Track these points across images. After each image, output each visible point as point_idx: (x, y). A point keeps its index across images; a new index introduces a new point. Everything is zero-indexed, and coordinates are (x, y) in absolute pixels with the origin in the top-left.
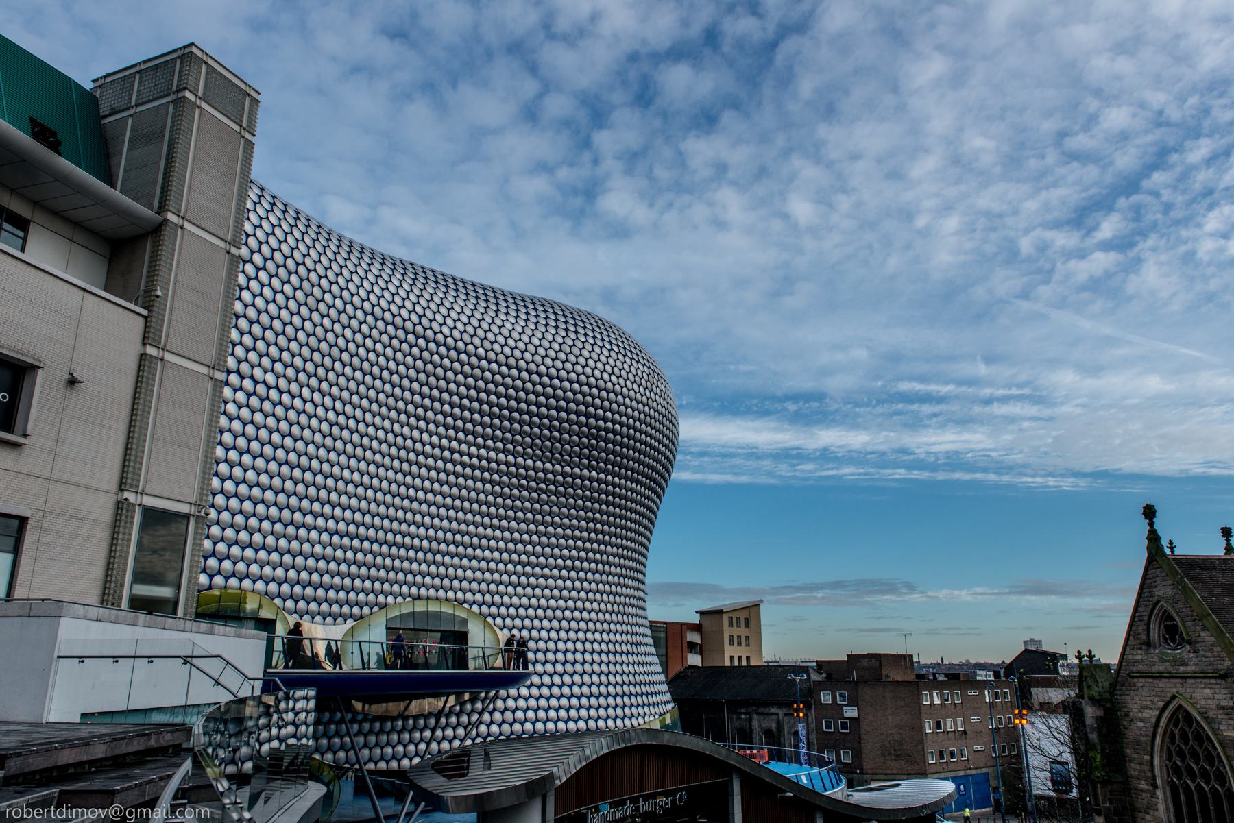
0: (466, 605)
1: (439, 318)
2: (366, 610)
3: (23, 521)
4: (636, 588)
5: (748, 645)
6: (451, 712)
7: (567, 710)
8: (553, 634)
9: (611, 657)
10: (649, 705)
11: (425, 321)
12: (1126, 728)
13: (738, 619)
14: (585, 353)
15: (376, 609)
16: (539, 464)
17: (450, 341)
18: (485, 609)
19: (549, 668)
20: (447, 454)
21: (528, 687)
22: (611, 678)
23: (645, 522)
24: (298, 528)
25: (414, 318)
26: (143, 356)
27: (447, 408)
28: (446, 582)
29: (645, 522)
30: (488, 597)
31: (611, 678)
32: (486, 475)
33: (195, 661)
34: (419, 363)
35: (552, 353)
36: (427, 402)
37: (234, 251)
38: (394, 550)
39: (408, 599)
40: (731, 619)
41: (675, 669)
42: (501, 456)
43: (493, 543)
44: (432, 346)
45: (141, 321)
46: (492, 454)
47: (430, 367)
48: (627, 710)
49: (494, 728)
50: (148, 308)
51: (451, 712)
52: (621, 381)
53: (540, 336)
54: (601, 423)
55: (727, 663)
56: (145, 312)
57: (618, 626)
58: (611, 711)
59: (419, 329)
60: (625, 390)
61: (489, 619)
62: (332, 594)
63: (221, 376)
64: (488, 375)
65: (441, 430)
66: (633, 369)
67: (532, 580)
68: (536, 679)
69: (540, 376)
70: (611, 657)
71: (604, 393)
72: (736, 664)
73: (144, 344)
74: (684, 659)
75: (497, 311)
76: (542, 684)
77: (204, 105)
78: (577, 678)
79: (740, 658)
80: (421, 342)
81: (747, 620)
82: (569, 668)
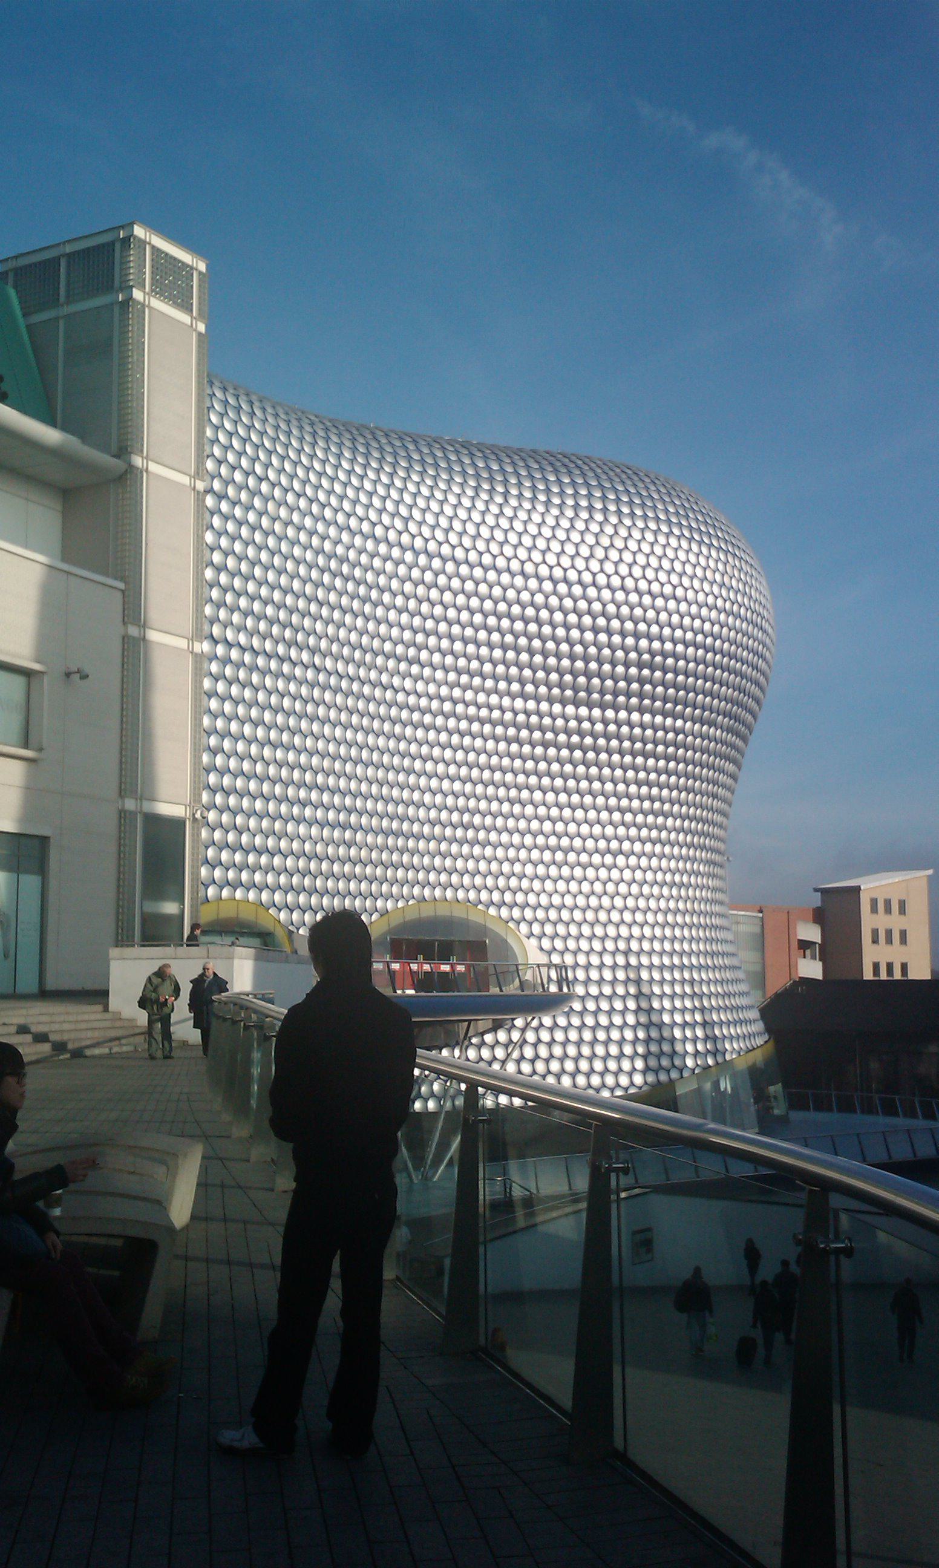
3: (44, 840)
21: (567, 1015)
23: (744, 714)
25: (399, 524)
26: (125, 638)
29: (744, 714)
33: (88, 1052)
40: (874, 903)
41: (777, 983)
45: (119, 595)
49: (562, 1021)
50: (122, 579)
55: (868, 975)
56: (122, 586)
61: (511, 925)
71: (660, 602)
72: (884, 976)
73: (124, 623)
74: (791, 966)
79: (890, 966)
80: (409, 557)
81: (903, 935)
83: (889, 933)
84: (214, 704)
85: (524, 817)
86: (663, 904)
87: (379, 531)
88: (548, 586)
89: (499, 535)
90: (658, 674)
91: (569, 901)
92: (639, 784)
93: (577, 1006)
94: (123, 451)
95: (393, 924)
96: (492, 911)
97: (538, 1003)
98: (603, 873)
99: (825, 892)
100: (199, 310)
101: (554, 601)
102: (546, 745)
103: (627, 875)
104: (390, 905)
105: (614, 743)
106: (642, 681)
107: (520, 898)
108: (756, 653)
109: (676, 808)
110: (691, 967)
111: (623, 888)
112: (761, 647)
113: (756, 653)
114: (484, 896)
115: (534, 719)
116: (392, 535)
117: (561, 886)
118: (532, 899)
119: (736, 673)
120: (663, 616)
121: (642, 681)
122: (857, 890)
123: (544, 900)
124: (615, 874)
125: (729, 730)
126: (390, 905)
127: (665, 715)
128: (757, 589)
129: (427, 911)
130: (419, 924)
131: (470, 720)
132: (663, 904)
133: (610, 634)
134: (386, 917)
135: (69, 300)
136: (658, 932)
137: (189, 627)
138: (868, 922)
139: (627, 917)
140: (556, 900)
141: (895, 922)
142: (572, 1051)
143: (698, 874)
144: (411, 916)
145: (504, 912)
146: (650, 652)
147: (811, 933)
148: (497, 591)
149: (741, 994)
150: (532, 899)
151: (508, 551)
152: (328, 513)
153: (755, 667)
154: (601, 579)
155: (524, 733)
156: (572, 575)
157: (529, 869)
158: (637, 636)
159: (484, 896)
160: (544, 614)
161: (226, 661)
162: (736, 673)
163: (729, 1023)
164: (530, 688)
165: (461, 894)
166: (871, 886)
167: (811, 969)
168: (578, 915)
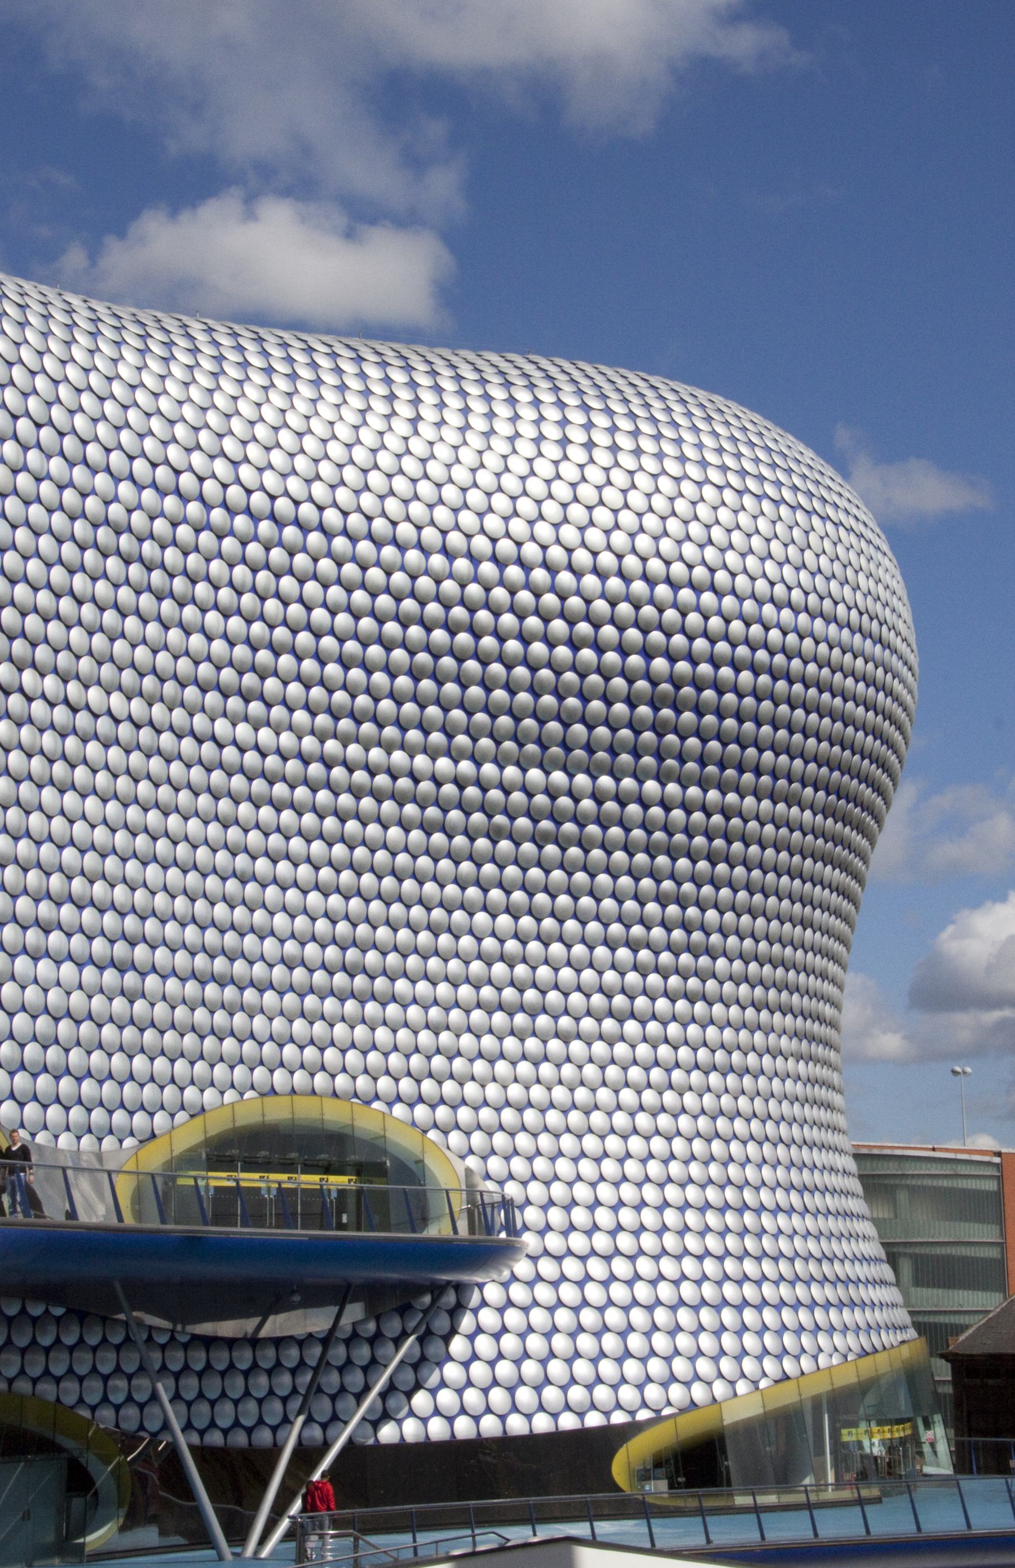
0: (376, 1105)
2: (160, 1118)
4: (799, 1057)
6: (353, 1339)
7: (623, 1335)
8: (586, 1167)
9: (748, 1218)
10: (832, 1329)
12: (72, 1214)
14: (636, 499)
15: (181, 1117)
16: (535, 774)
18: (421, 1112)
19: (578, 1242)
20: (315, 769)
24: (665, 1024)
27: (309, 665)
31: (730, 1265)
32: (410, 809)
35: (551, 509)
38: (211, 990)
39: (249, 1095)
42: (444, 764)
46: (421, 761)
47: (240, 572)
48: (788, 1339)
51: (353, 1339)
57: (781, 1149)
58: (728, 1341)
59: (234, 492)
60: (741, 581)
62: (88, 1087)
64: (375, 574)
65: (300, 716)
67: (360, 1032)
69: (475, 560)
71: (686, 595)
75: (415, 421)
76: (563, 1278)
78: (645, 1266)
82: (625, 1242)
85: (686, 1043)
88: (488, 569)
90: (688, 716)
92: (663, 901)
93: (522, 1268)
95: (213, 1132)
96: (399, 1110)
98: (599, 1048)
102: (494, 835)
103: (643, 1050)
104: (210, 1096)
105: (615, 832)
106: (659, 729)
107: (449, 1088)
108: (871, 683)
109: (732, 940)
110: (760, 1209)
112: (880, 671)
113: (871, 683)
115: (472, 792)
117: (524, 1068)
119: (833, 715)
120: (721, 576)
121: (659, 729)
123: (492, 1091)
124: (621, 1049)
125: (826, 812)
127: (704, 785)
128: (894, 610)
131: (357, 794)
133: (600, 650)
134: (199, 1120)
143: (775, 1053)
146: (672, 679)
149: (864, 1259)
150: (471, 1090)
153: (869, 706)
162: (833, 715)
163: (828, 1305)
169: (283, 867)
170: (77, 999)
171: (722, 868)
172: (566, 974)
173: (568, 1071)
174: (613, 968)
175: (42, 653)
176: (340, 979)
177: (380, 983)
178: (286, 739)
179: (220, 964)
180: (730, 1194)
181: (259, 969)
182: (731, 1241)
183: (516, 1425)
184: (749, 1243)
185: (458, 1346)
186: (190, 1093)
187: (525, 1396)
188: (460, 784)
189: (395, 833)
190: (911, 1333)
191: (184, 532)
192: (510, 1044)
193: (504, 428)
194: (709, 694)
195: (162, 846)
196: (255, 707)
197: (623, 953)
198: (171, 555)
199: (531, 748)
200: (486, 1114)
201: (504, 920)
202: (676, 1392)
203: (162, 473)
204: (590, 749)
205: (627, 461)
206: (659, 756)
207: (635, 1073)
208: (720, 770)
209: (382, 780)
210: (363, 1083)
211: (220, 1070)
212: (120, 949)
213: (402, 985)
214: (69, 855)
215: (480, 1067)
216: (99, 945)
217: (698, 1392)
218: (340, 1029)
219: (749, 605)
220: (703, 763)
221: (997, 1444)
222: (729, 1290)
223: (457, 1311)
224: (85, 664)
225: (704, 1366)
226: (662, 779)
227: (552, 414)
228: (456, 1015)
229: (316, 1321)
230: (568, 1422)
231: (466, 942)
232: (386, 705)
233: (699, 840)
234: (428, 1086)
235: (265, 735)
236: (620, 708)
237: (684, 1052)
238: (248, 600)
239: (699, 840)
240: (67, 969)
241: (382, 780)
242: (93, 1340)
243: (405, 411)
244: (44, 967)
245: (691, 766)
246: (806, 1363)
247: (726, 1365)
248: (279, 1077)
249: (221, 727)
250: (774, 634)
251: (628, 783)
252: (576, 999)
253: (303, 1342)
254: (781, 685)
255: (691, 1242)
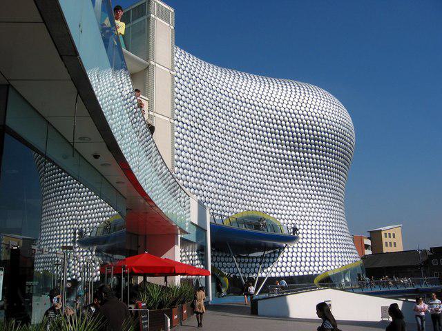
1: (246, 92)
5: (395, 246)
11: (241, 94)
13: (390, 234)
17: (251, 102)
20: (254, 150)
22: (332, 245)
28: (259, 204)
30: (276, 211)
31: (332, 245)
34: (240, 112)
36: (244, 128)
37: (172, 73)
40: (386, 234)
42: (277, 150)
43: (276, 188)
44: (244, 104)
47: (244, 113)
52: (327, 113)
53: (286, 103)
54: (319, 133)
59: (239, 97)
63: (174, 73)
65: (251, 140)
66: (332, 108)
68: (301, 241)
70: (334, 237)
71: (319, 120)
77: (158, 18)
80: (240, 103)
81: (395, 243)
83: (390, 243)
84: (179, 163)
86: (326, 215)
87: (230, 95)
89: (268, 98)
91: (296, 213)
93: (301, 241)
94: (148, 59)
96: (271, 215)
97: (291, 239)
98: (306, 205)
99: (371, 232)
100: (172, 21)
101: (286, 118)
103: (314, 205)
104: (238, 210)
107: (280, 211)
111: (313, 210)
114: (268, 210)
116: (234, 96)
117: (293, 208)
118: (284, 212)
120: (321, 124)
122: (381, 230)
123: (288, 212)
124: (310, 205)
126: (238, 210)
129: (250, 214)
130: (248, 217)
132: (326, 215)
135: (133, 20)
136: (325, 223)
137: (170, 116)
138: (384, 240)
139: (315, 218)
140: (292, 213)
141: (392, 240)
142: (299, 259)
144: (245, 215)
145: (275, 216)
147: (368, 242)
148: (268, 115)
150: (284, 212)
151: (271, 103)
152: (214, 87)
154: (301, 112)
155: (279, 160)
156: (291, 111)
157: (283, 203)
158: (313, 130)
159: (268, 210)
160: (283, 122)
161: (182, 128)
164: (280, 146)
165: (261, 209)
166: (385, 229)
167: (368, 252)
168: (299, 217)
169: (249, 168)
170: (214, 190)
171: (326, 171)
172: (300, 191)
173: (301, 209)
174: (308, 190)
175: (206, 123)
176: (260, 190)
177: (267, 191)
178: (249, 144)
179: (239, 185)
180: (331, 232)
181: (246, 187)
182: (332, 241)
183: (296, 274)
184: (335, 241)
185: (280, 259)
186: (235, 209)
187: (298, 269)
188: (280, 154)
189: (268, 163)
190: (359, 259)
191: (230, 104)
192: (290, 204)
193: (285, 89)
194: (324, 138)
195: (228, 162)
196: (243, 138)
197: (310, 187)
198: (228, 108)
199: (292, 148)
200: (287, 217)
201: (288, 180)
202: (325, 268)
203: (226, 93)
204: (303, 148)
205: (307, 96)
206: (315, 150)
207: (313, 210)
208: (326, 153)
209: (266, 153)
210: (265, 210)
211: (240, 206)
212: (222, 181)
213: (271, 192)
214: (212, 162)
215: (285, 208)
216: (218, 180)
217: (329, 268)
218: (260, 199)
219: (329, 130)
220: (323, 151)
221: (206, 247)
222: (332, 250)
223: (279, 253)
224: (214, 126)
225: (329, 263)
226: (316, 154)
227: (293, 87)
228: (280, 198)
229: (260, 254)
230: (306, 273)
231: (282, 184)
232: (266, 139)
233: (322, 166)
234: (276, 211)
235: (245, 143)
236: (308, 140)
237: (321, 206)
238: (242, 117)
239: (322, 166)
240: (213, 184)
241: (266, 153)
242: (224, 255)
243: (267, 85)
244: (209, 183)
245: (321, 152)
246: (346, 263)
247: (333, 263)
248: (250, 208)
249: (237, 141)
250: (335, 128)
251: (310, 155)
252: (302, 195)
253: (257, 258)
254: (336, 137)
255: (325, 241)
